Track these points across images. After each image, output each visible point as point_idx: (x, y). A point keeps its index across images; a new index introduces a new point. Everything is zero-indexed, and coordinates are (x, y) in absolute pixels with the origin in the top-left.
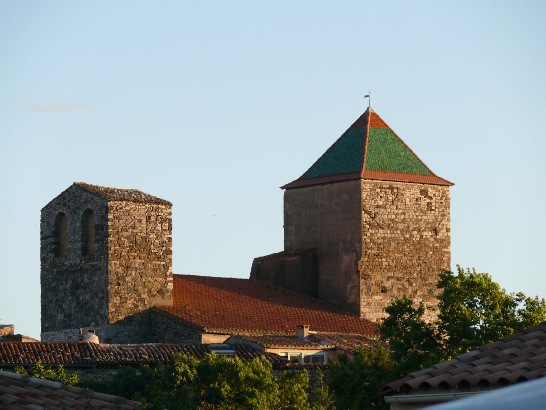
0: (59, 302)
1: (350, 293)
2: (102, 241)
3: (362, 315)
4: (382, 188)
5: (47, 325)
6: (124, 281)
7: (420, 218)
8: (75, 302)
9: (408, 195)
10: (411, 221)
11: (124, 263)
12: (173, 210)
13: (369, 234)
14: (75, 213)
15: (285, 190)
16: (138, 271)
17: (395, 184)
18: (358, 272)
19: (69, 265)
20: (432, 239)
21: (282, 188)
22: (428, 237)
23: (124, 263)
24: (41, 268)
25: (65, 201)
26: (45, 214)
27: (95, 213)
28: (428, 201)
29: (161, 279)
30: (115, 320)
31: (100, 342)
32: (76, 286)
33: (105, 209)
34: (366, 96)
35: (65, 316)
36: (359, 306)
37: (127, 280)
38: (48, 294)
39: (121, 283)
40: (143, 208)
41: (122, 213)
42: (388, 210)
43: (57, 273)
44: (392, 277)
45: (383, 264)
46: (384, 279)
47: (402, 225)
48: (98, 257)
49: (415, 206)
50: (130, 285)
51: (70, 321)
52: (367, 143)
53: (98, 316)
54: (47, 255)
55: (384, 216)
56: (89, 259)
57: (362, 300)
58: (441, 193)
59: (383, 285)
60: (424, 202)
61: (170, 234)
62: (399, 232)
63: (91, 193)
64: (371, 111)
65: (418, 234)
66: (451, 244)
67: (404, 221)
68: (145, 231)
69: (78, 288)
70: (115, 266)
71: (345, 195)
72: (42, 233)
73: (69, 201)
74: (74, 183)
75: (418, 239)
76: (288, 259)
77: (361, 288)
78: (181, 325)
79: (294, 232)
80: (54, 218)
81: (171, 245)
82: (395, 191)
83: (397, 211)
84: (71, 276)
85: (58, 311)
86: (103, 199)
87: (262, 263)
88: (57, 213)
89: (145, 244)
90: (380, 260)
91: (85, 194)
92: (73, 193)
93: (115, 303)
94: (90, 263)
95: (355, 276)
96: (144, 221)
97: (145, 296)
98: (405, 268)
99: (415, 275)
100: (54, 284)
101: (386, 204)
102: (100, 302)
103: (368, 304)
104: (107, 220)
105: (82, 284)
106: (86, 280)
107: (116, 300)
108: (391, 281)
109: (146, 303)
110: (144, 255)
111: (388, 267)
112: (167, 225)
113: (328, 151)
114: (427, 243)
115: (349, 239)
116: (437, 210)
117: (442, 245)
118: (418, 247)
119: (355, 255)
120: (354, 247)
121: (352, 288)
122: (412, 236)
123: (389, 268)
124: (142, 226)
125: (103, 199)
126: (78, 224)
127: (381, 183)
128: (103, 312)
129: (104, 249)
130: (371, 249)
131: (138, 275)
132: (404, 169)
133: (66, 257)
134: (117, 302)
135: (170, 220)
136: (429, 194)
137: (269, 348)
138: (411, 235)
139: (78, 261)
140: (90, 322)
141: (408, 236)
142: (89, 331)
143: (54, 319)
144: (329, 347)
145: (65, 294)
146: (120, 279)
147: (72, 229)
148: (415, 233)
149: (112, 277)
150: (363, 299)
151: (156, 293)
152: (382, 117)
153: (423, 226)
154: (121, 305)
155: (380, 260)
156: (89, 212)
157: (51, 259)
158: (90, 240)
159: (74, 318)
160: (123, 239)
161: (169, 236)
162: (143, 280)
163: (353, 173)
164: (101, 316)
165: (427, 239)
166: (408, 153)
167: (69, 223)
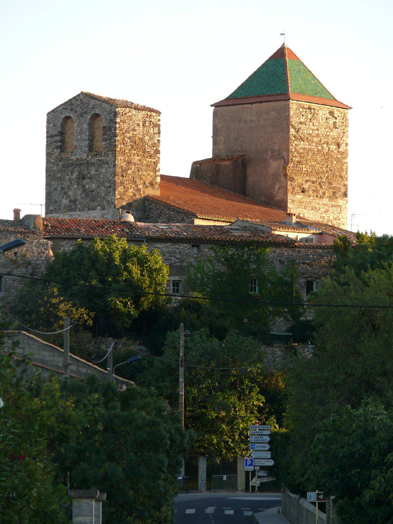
0: (64, 189)
1: (277, 192)
2: (110, 140)
3: (288, 210)
4: (303, 108)
5: (51, 208)
6: (127, 174)
7: (328, 133)
8: (81, 190)
9: (321, 115)
10: (323, 136)
11: (127, 158)
12: (162, 117)
13: (294, 145)
14: (82, 116)
15: (214, 107)
16: (137, 166)
17: (313, 106)
18: (286, 175)
19: (75, 159)
20: (336, 152)
21: (212, 106)
22: (334, 149)
23: (127, 158)
24: (46, 162)
25: (72, 107)
26: (51, 117)
27: (103, 117)
28: (334, 120)
29: (152, 173)
30: (120, 205)
31: (135, 221)
32: (82, 177)
33: (113, 114)
34: (281, 34)
35: (70, 201)
36: (286, 202)
37: (129, 173)
38: (53, 182)
39: (124, 175)
40: (141, 115)
41: (126, 118)
42: (307, 126)
43: (63, 166)
44: (309, 181)
45: (303, 170)
46: (304, 182)
47: (316, 139)
48: (105, 153)
49: (325, 124)
50: (130, 177)
51: (76, 205)
52: (288, 72)
53: (104, 202)
54: (53, 151)
55: (305, 130)
56: (96, 155)
57: (289, 198)
58: (343, 115)
59: (303, 187)
60: (331, 121)
61: (159, 137)
62: (314, 144)
63: (99, 100)
64: (286, 47)
65: (327, 147)
66: (348, 156)
67: (318, 135)
68: (142, 134)
69: (84, 178)
70: (120, 161)
71: (273, 113)
72: (47, 132)
73: (76, 107)
74: (82, 92)
75: (327, 151)
76: (223, 163)
77: (289, 188)
78: (174, 211)
79: (222, 142)
80: (61, 121)
81: (159, 146)
82: (312, 111)
83: (313, 127)
84: (77, 168)
85: (63, 197)
86: (111, 106)
87: (201, 165)
88: (63, 116)
89: (141, 144)
90: (301, 166)
91: (93, 101)
92: (81, 100)
93: (120, 191)
94: (97, 158)
95: (283, 178)
96: (141, 125)
97: (141, 186)
98: (318, 174)
99: (324, 180)
100: (59, 175)
101: (306, 121)
102: (107, 190)
103: (293, 201)
104: (116, 123)
105: (89, 175)
106: (93, 172)
107: (120, 189)
108: (309, 183)
109: (141, 192)
110: (141, 153)
111: (306, 172)
112: (157, 129)
113: (250, 77)
114: (333, 154)
115: (277, 148)
116: (340, 128)
117: (343, 156)
118: (327, 157)
119: (283, 162)
120: (282, 154)
121: (279, 188)
122: (322, 147)
123: (307, 174)
124: (140, 129)
125: (111, 106)
126: (85, 126)
127: (303, 104)
128: (109, 198)
129: (112, 148)
130: (296, 157)
131: (136, 169)
132: (316, 93)
133: (72, 153)
134: (122, 191)
135: (159, 125)
136: (336, 115)
137: (276, 230)
138: (322, 147)
139: (85, 156)
140: (96, 207)
141: (320, 148)
142: (127, 212)
143: (58, 204)
144: (318, 232)
145: (71, 183)
146: (125, 171)
147: (79, 129)
148: (325, 146)
149: (118, 170)
150: (290, 197)
151: (148, 184)
152: (294, 51)
153: (330, 140)
154: (125, 193)
155: (301, 166)
156: (96, 116)
157: (57, 154)
158: (96, 139)
159: (80, 203)
160: (126, 139)
161: (158, 139)
162: (140, 174)
163: (280, 95)
164: (108, 201)
165: (332, 151)
166: (316, 81)
167: (76, 125)
